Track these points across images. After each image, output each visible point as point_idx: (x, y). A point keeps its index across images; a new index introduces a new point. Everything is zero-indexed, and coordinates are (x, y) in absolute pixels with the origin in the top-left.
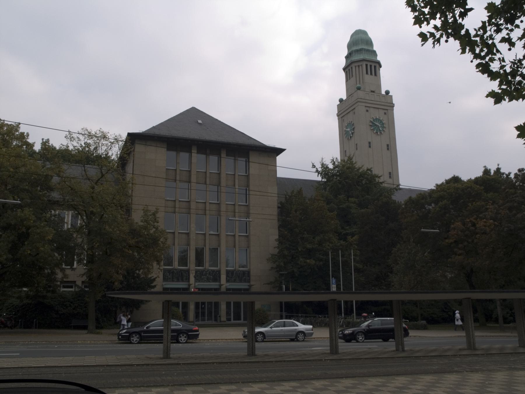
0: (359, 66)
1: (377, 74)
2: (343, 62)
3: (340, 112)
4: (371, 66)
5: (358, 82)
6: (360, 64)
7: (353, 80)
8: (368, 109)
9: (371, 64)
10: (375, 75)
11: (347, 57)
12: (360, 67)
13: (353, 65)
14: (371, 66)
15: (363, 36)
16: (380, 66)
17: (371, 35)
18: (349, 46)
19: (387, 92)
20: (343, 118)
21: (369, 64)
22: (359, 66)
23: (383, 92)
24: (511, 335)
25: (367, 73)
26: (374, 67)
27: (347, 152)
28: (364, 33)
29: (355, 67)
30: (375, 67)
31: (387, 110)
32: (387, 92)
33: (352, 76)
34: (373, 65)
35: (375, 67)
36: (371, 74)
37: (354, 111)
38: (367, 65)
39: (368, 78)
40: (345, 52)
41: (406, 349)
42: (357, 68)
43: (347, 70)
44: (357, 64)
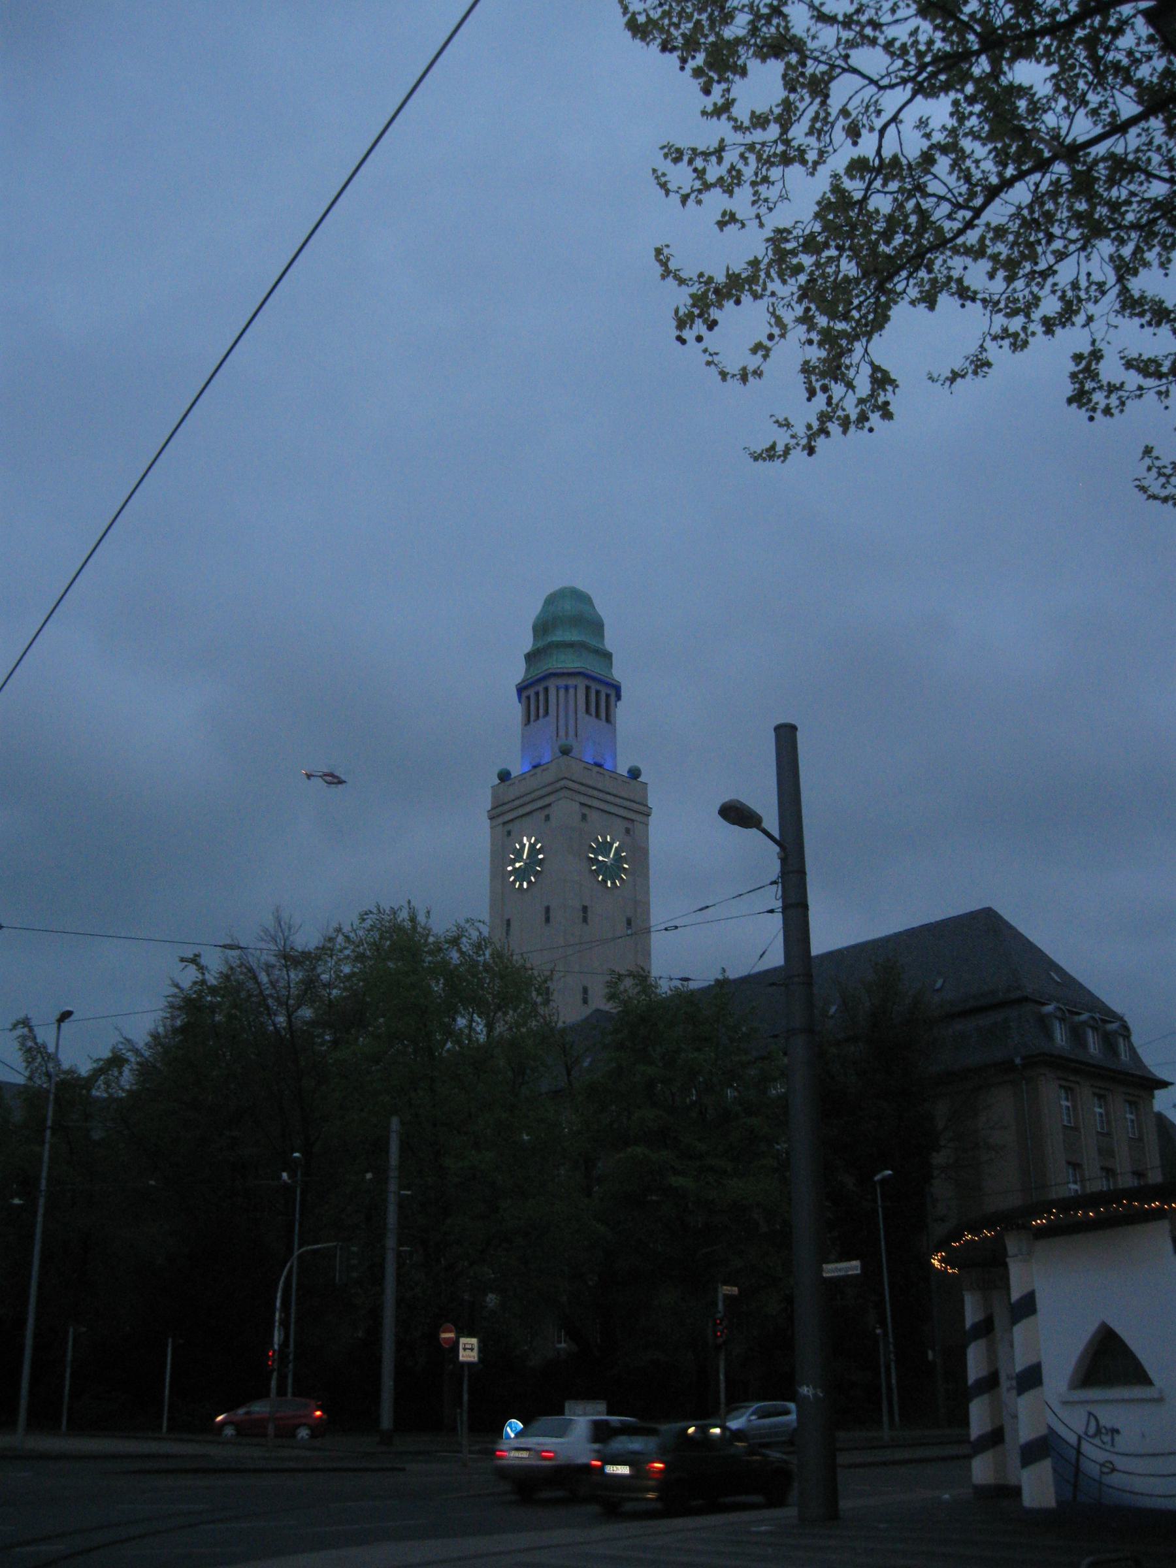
0: (567, 688)
1: (612, 719)
2: (518, 672)
3: (499, 810)
4: (598, 692)
5: (562, 733)
6: (571, 682)
7: (546, 726)
8: (586, 811)
9: (599, 687)
10: (608, 720)
11: (530, 658)
12: (572, 691)
13: (552, 684)
14: (598, 692)
15: (568, 607)
16: (619, 697)
17: (603, 608)
18: (542, 628)
19: (635, 774)
20: (509, 827)
21: (594, 687)
22: (567, 688)
23: (623, 770)
24: (1159, 1500)
25: (588, 711)
26: (603, 696)
27: (513, 923)
28: (582, 598)
29: (558, 689)
30: (608, 696)
31: (633, 821)
32: (635, 774)
33: (547, 713)
34: (604, 691)
35: (608, 696)
36: (598, 716)
37: (546, 812)
38: (588, 688)
39: (588, 723)
40: (527, 643)
41: (844, 1504)
42: (562, 692)
43: (531, 692)
44: (561, 682)
